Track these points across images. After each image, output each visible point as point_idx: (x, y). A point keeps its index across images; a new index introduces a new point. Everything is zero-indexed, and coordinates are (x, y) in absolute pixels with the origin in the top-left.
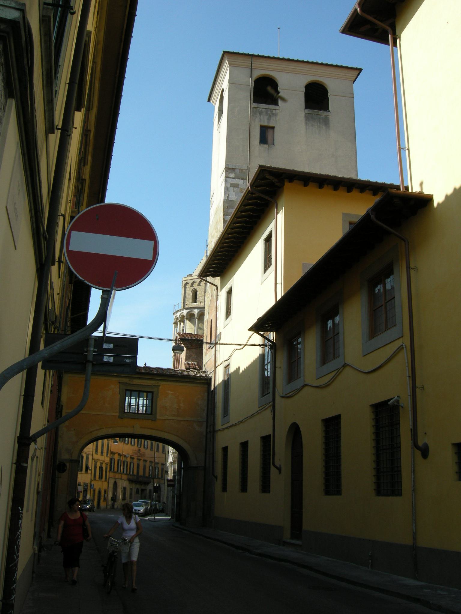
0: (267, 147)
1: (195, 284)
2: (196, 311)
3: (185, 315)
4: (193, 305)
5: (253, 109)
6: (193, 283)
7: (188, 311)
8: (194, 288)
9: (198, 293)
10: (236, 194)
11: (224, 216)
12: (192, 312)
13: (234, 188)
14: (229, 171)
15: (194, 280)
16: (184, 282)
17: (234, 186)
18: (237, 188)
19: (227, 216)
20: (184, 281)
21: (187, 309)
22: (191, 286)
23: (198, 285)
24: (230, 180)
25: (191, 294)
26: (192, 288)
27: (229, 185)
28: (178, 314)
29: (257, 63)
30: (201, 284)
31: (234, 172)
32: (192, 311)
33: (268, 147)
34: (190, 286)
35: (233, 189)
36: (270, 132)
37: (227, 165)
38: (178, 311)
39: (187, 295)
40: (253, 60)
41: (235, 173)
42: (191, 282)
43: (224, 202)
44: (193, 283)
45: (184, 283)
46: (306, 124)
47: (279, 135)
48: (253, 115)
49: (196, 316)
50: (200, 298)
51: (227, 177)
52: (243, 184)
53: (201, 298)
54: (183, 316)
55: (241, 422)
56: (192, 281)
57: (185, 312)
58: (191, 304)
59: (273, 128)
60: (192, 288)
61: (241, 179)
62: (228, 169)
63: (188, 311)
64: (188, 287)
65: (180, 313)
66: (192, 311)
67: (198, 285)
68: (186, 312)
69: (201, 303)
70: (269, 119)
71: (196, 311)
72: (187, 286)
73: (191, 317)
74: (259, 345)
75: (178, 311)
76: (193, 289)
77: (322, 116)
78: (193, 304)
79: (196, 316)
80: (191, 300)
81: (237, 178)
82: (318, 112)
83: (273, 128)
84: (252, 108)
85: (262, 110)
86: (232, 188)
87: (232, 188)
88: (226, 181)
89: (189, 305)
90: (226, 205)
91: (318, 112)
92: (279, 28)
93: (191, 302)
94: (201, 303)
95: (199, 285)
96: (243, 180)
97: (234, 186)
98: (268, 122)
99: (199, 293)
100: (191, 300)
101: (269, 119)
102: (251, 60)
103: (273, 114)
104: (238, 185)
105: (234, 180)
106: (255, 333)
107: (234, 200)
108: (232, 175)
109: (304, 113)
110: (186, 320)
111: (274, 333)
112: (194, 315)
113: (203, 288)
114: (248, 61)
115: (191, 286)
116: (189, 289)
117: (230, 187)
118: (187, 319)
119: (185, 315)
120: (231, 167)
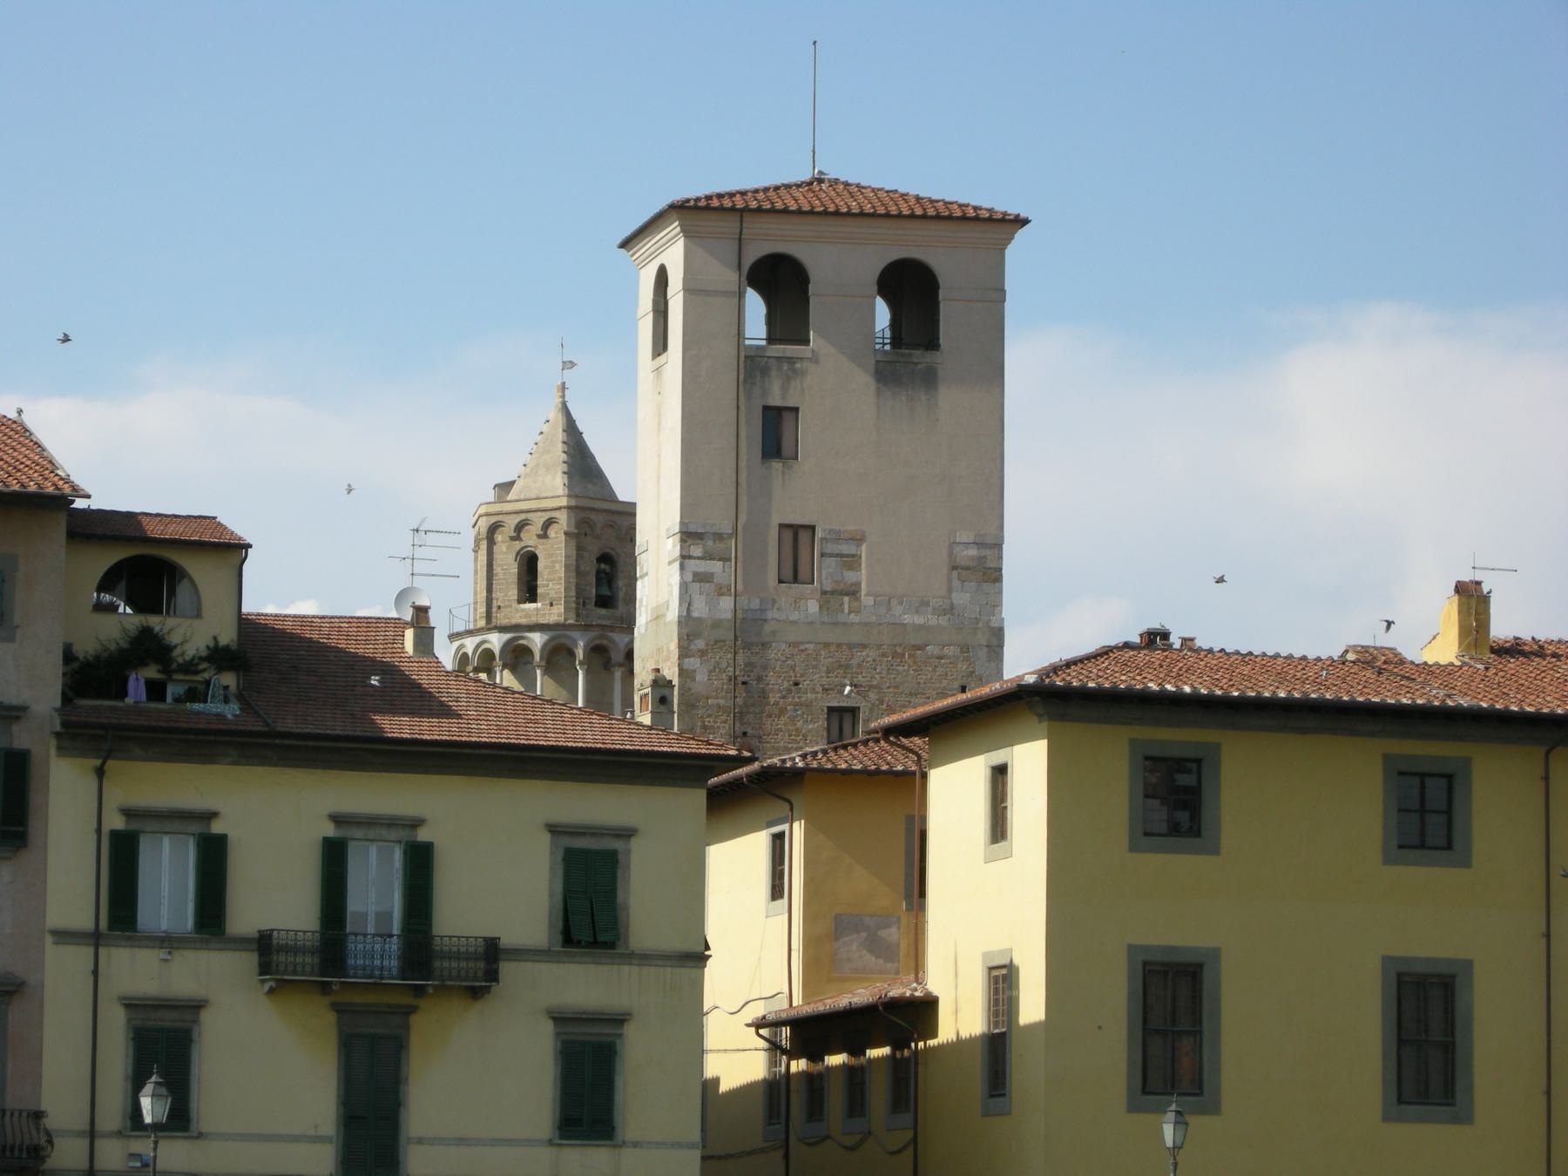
0: (781, 468)
1: (528, 531)
2: (537, 640)
3: (497, 652)
4: (523, 610)
5: (745, 361)
6: (520, 527)
7: (506, 636)
8: (523, 544)
9: (541, 565)
10: (706, 599)
11: (679, 658)
12: (521, 642)
13: (702, 584)
14: (690, 542)
15: (523, 516)
16: (484, 506)
17: (701, 578)
18: (708, 584)
19: (687, 660)
20: (488, 514)
21: (502, 629)
22: (513, 539)
23: (539, 536)
24: (693, 565)
25: (514, 569)
26: (517, 545)
27: (689, 578)
28: (470, 644)
29: (753, 226)
30: (552, 532)
31: (700, 542)
32: (523, 638)
33: (783, 466)
34: (508, 539)
35: (701, 587)
36: (787, 418)
37: (684, 523)
38: (470, 633)
39: (497, 570)
40: (744, 219)
41: (704, 545)
42: (512, 522)
43: (680, 623)
44: (520, 527)
45: (484, 524)
46: (878, 391)
47: (808, 433)
48: (745, 381)
49: (537, 657)
50: (548, 586)
51: (685, 557)
52: (724, 571)
53: (551, 586)
54: (488, 655)
55: (732, 1156)
56: (515, 520)
57: (496, 641)
58: (515, 605)
59: (796, 410)
60: (517, 545)
61: (719, 560)
62: (688, 536)
63: (506, 636)
64: (503, 542)
65: (478, 639)
66: (523, 638)
67: (539, 536)
68: (499, 640)
69: (551, 605)
70: (785, 390)
71: (537, 640)
72: (499, 537)
73: (516, 658)
74: (764, 1050)
75: (470, 633)
76: (523, 548)
77: (920, 366)
78: (523, 606)
79: (537, 657)
80: (516, 592)
81: (708, 556)
82: (910, 355)
83: (796, 410)
84: (742, 359)
85: (767, 362)
86: (697, 585)
87: (698, 584)
88: (682, 567)
89: (509, 609)
90: (685, 631)
91: (910, 355)
92: (815, 43)
93: (516, 598)
94: (551, 605)
95: (544, 535)
96: (721, 563)
97: (701, 578)
98: (783, 397)
99: (546, 567)
100: (513, 593)
101: (785, 390)
102: (738, 225)
103: (795, 371)
104: (712, 575)
105: (702, 562)
106: (746, 336)
107: (704, 616)
108: (697, 551)
109: (874, 362)
110: (501, 671)
111: (788, 1028)
112: (527, 651)
113: (559, 549)
114: (730, 225)
115: (513, 539)
116: (504, 549)
117: (693, 581)
118: (505, 666)
119: (497, 652)
120: (692, 528)
